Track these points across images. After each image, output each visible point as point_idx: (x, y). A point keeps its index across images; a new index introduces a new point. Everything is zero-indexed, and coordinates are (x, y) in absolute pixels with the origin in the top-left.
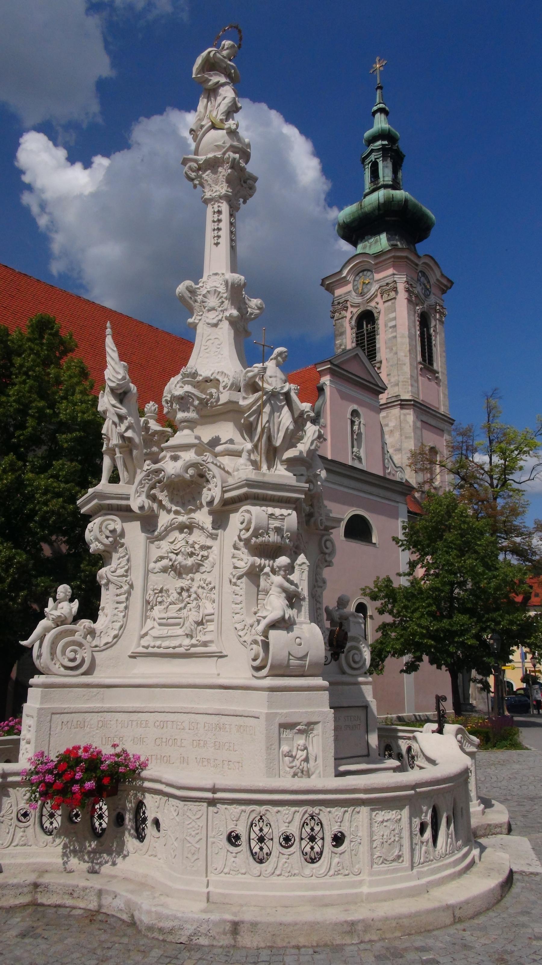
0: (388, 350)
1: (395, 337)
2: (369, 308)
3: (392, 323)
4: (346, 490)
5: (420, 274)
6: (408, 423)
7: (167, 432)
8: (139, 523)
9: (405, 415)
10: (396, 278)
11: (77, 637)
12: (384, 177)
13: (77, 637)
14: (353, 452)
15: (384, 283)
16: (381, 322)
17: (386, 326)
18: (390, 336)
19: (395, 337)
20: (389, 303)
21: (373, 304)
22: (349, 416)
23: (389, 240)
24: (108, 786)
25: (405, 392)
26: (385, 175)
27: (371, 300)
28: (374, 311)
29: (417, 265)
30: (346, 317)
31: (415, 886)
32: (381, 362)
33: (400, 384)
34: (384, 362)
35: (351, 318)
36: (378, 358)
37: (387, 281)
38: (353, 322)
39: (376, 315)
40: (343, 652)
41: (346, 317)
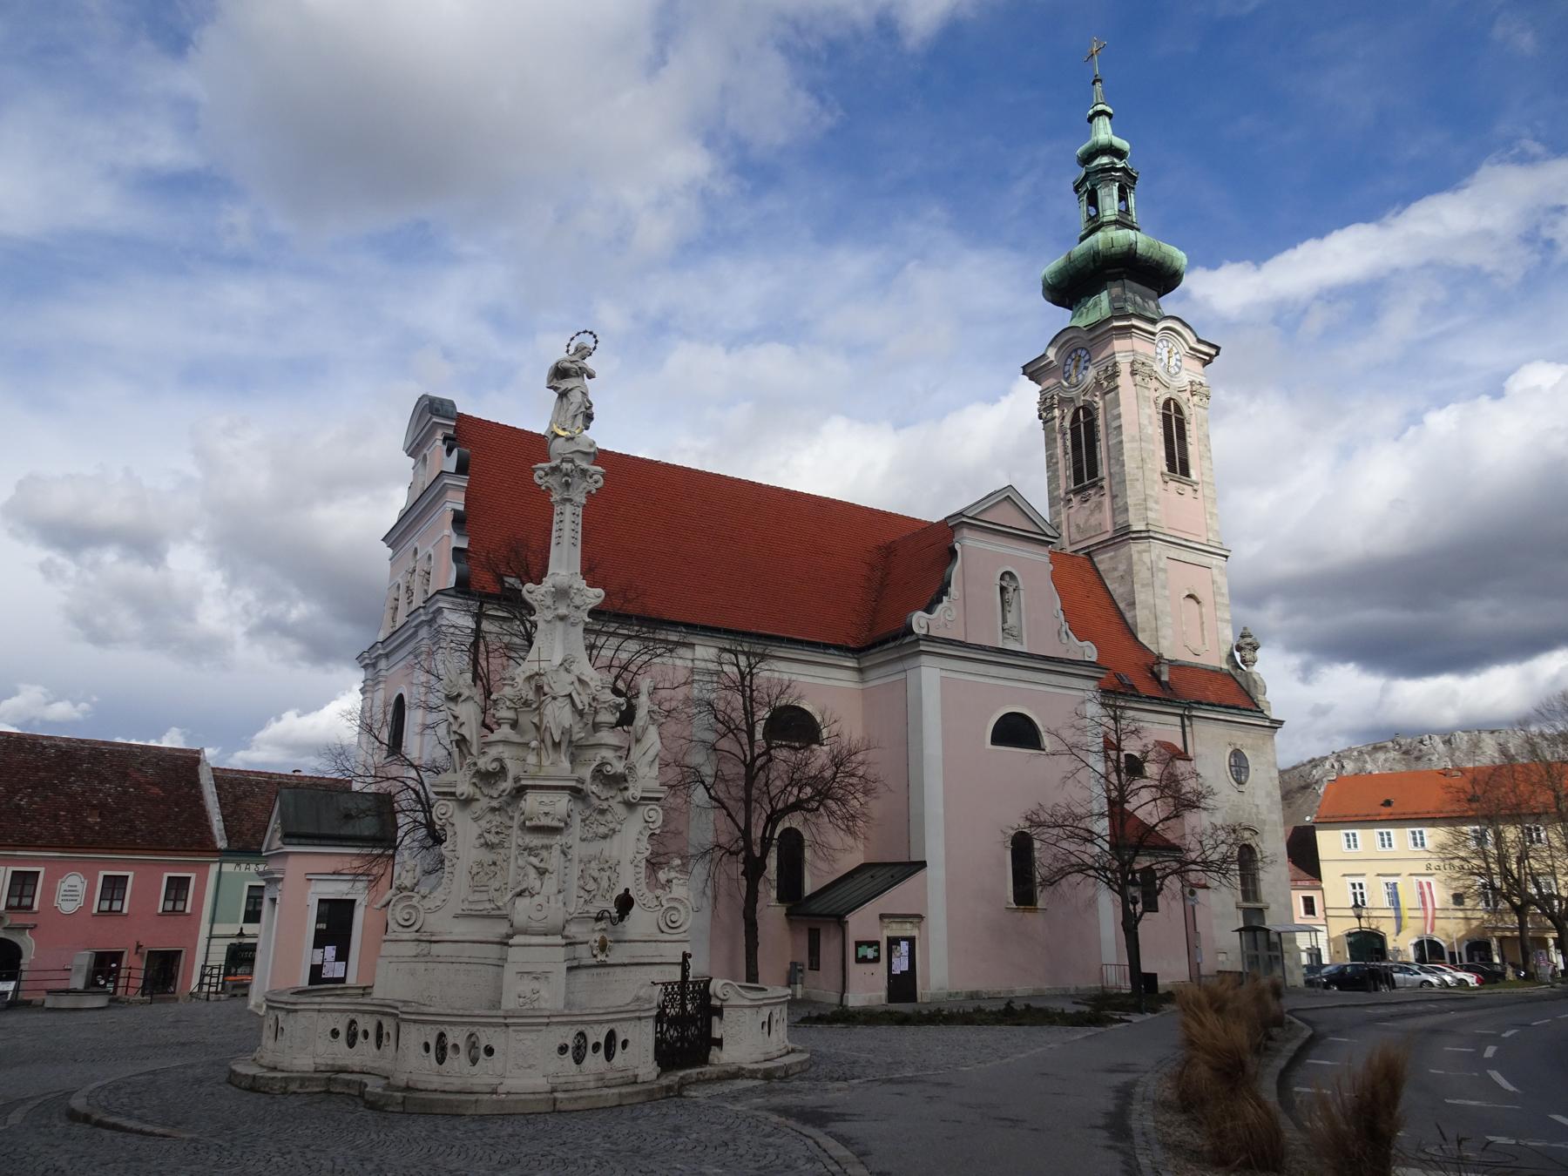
3: (1115, 424)
4: (993, 681)
11: (414, 902)
13: (414, 902)
22: (998, 581)
29: (1153, 334)
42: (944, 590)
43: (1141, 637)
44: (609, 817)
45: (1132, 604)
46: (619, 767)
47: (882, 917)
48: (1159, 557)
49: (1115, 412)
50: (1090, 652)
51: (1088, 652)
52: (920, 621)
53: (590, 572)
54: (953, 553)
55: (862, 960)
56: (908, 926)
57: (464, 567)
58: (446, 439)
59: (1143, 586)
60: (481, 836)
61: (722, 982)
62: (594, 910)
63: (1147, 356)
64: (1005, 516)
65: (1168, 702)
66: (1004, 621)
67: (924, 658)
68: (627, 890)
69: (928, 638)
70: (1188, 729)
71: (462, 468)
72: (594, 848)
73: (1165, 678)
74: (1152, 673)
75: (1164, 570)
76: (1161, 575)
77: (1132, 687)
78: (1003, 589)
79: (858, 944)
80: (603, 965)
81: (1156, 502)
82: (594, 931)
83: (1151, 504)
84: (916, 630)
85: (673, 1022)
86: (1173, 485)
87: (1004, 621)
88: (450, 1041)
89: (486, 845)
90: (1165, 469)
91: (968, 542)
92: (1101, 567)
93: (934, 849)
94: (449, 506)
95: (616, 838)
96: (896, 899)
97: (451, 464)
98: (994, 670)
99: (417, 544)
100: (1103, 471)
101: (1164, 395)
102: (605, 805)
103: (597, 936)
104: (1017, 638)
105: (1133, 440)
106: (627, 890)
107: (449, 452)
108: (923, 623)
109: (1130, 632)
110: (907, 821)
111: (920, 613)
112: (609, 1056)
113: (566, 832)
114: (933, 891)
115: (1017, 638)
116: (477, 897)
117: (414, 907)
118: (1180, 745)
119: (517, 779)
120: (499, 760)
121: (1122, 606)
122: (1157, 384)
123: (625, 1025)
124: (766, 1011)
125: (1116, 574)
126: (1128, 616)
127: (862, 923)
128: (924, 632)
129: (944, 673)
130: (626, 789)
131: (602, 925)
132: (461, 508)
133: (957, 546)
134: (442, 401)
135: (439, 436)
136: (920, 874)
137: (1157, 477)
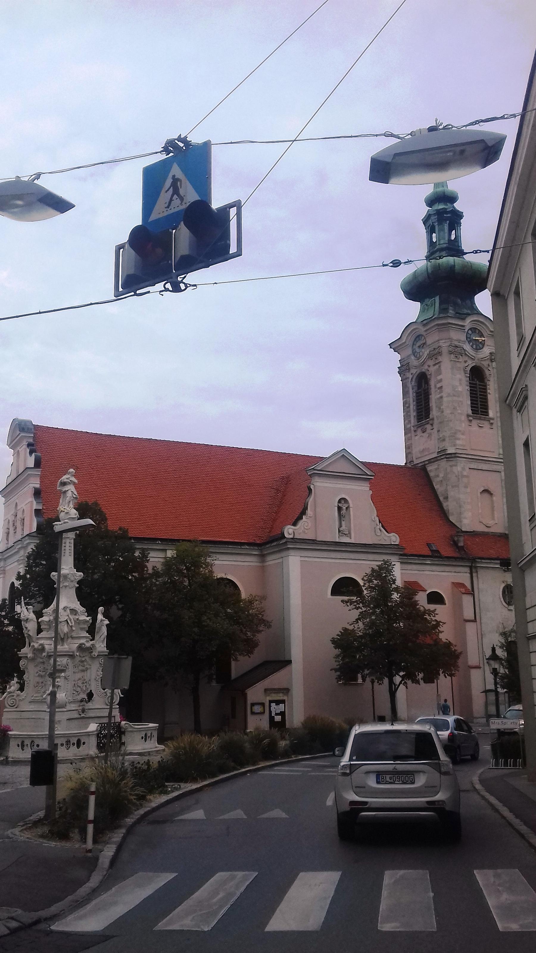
0: (437, 409)
1: (441, 397)
2: (424, 370)
3: (439, 385)
4: (333, 561)
5: (470, 332)
6: (454, 473)
7: (342, 755)
8: (430, 924)
9: (451, 466)
10: (441, 343)
11: (14, 697)
12: (439, 240)
13: (14, 697)
14: (339, 531)
15: (432, 349)
16: (432, 383)
17: (435, 386)
18: (438, 396)
19: (441, 397)
20: (437, 366)
21: (426, 367)
23: (440, 304)
24: (392, 602)
25: (451, 446)
26: (441, 238)
27: (424, 363)
28: (427, 373)
30: (408, 378)
31: (388, 788)
32: (433, 419)
33: (447, 439)
34: (435, 419)
35: (412, 378)
36: (431, 416)
37: (434, 347)
38: (413, 383)
39: (428, 377)
40: (148, 763)
41: (408, 378)
42: (304, 512)
43: (452, 519)
44: (85, 663)
45: (446, 498)
46: (88, 645)
47: (266, 690)
48: (463, 469)
49: (439, 378)
50: (394, 539)
51: (393, 539)
52: (289, 531)
53: (78, 566)
54: (310, 490)
55: (253, 713)
56: (281, 695)
57: (39, 519)
58: (29, 445)
59: (453, 487)
60: (37, 672)
61: (125, 722)
62: (79, 698)
63: (459, 341)
64: (343, 467)
65: (462, 559)
66: (340, 526)
67: (292, 552)
68: (91, 691)
69: (294, 540)
70: (474, 575)
71: (38, 464)
72: (79, 675)
73: (461, 544)
74: (454, 541)
75: (467, 477)
76: (465, 480)
77: (437, 551)
78: (340, 509)
79: (253, 705)
80: (83, 718)
81: (463, 434)
82: (80, 706)
83: (459, 436)
84: (286, 535)
85: (105, 736)
86: (475, 422)
87: (340, 526)
88: (25, 743)
89: (39, 676)
90: (470, 412)
91: (318, 484)
92: (432, 474)
93: (296, 652)
94: (32, 486)
95: (88, 671)
96: (276, 680)
97: (31, 461)
98: (333, 555)
99: (17, 501)
100: (434, 413)
101: (471, 364)
102: (83, 659)
103: (81, 708)
104: (349, 535)
105: (449, 395)
106: (91, 691)
107: (31, 453)
108: (291, 531)
109: (444, 514)
110: (282, 641)
111: (289, 526)
112: (78, 747)
113: (67, 670)
114: (296, 675)
115: (349, 535)
116: (37, 695)
117: (15, 699)
118: (468, 585)
119: (48, 653)
120: (41, 645)
121: (441, 498)
122: (466, 358)
123: (84, 737)
124: (144, 733)
125: (439, 479)
126: (445, 505)
127: (255, 694)
128: (291, 536)
129: (303, 559)
130: (92, 652)
131: (82, 703)
132: (38, 486)
133: (312, 487)
134: (26, 422)
135: (25, 443)
136: (287, 668)
137: (464, 418)
